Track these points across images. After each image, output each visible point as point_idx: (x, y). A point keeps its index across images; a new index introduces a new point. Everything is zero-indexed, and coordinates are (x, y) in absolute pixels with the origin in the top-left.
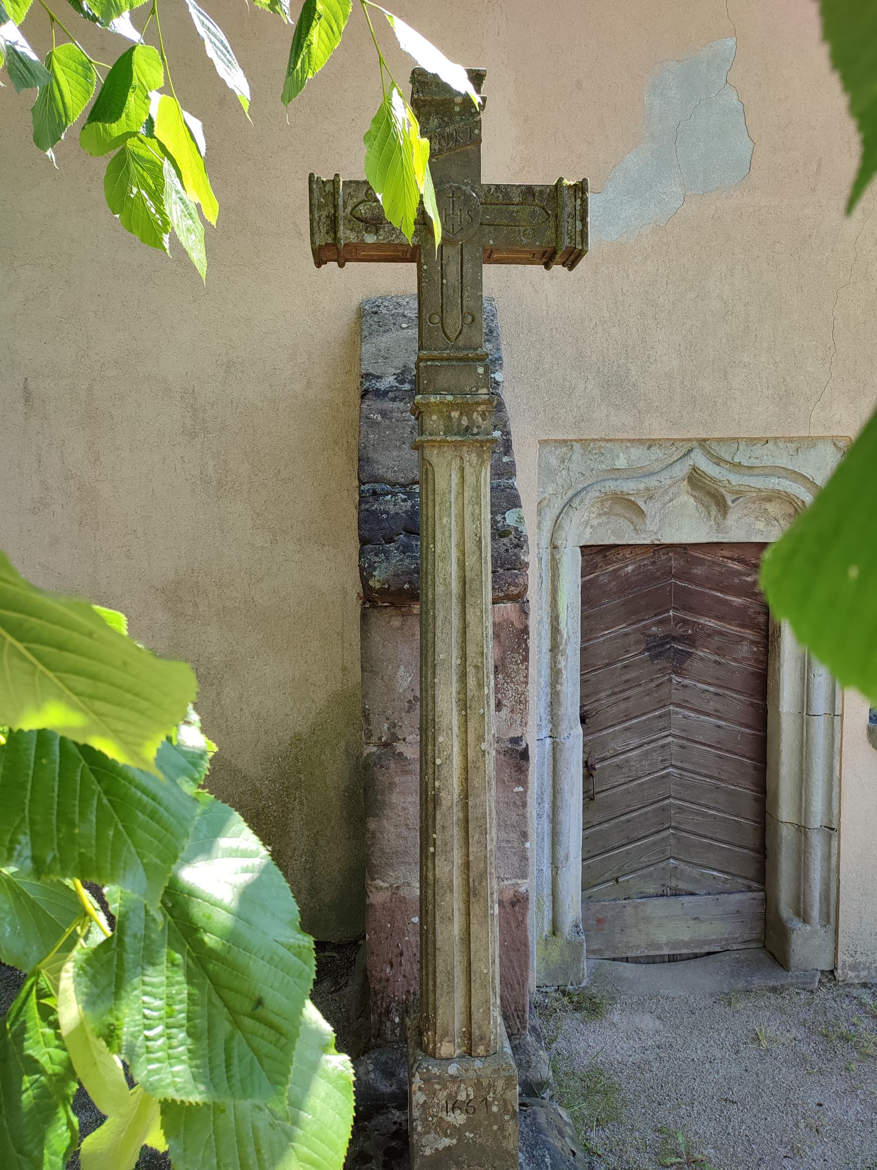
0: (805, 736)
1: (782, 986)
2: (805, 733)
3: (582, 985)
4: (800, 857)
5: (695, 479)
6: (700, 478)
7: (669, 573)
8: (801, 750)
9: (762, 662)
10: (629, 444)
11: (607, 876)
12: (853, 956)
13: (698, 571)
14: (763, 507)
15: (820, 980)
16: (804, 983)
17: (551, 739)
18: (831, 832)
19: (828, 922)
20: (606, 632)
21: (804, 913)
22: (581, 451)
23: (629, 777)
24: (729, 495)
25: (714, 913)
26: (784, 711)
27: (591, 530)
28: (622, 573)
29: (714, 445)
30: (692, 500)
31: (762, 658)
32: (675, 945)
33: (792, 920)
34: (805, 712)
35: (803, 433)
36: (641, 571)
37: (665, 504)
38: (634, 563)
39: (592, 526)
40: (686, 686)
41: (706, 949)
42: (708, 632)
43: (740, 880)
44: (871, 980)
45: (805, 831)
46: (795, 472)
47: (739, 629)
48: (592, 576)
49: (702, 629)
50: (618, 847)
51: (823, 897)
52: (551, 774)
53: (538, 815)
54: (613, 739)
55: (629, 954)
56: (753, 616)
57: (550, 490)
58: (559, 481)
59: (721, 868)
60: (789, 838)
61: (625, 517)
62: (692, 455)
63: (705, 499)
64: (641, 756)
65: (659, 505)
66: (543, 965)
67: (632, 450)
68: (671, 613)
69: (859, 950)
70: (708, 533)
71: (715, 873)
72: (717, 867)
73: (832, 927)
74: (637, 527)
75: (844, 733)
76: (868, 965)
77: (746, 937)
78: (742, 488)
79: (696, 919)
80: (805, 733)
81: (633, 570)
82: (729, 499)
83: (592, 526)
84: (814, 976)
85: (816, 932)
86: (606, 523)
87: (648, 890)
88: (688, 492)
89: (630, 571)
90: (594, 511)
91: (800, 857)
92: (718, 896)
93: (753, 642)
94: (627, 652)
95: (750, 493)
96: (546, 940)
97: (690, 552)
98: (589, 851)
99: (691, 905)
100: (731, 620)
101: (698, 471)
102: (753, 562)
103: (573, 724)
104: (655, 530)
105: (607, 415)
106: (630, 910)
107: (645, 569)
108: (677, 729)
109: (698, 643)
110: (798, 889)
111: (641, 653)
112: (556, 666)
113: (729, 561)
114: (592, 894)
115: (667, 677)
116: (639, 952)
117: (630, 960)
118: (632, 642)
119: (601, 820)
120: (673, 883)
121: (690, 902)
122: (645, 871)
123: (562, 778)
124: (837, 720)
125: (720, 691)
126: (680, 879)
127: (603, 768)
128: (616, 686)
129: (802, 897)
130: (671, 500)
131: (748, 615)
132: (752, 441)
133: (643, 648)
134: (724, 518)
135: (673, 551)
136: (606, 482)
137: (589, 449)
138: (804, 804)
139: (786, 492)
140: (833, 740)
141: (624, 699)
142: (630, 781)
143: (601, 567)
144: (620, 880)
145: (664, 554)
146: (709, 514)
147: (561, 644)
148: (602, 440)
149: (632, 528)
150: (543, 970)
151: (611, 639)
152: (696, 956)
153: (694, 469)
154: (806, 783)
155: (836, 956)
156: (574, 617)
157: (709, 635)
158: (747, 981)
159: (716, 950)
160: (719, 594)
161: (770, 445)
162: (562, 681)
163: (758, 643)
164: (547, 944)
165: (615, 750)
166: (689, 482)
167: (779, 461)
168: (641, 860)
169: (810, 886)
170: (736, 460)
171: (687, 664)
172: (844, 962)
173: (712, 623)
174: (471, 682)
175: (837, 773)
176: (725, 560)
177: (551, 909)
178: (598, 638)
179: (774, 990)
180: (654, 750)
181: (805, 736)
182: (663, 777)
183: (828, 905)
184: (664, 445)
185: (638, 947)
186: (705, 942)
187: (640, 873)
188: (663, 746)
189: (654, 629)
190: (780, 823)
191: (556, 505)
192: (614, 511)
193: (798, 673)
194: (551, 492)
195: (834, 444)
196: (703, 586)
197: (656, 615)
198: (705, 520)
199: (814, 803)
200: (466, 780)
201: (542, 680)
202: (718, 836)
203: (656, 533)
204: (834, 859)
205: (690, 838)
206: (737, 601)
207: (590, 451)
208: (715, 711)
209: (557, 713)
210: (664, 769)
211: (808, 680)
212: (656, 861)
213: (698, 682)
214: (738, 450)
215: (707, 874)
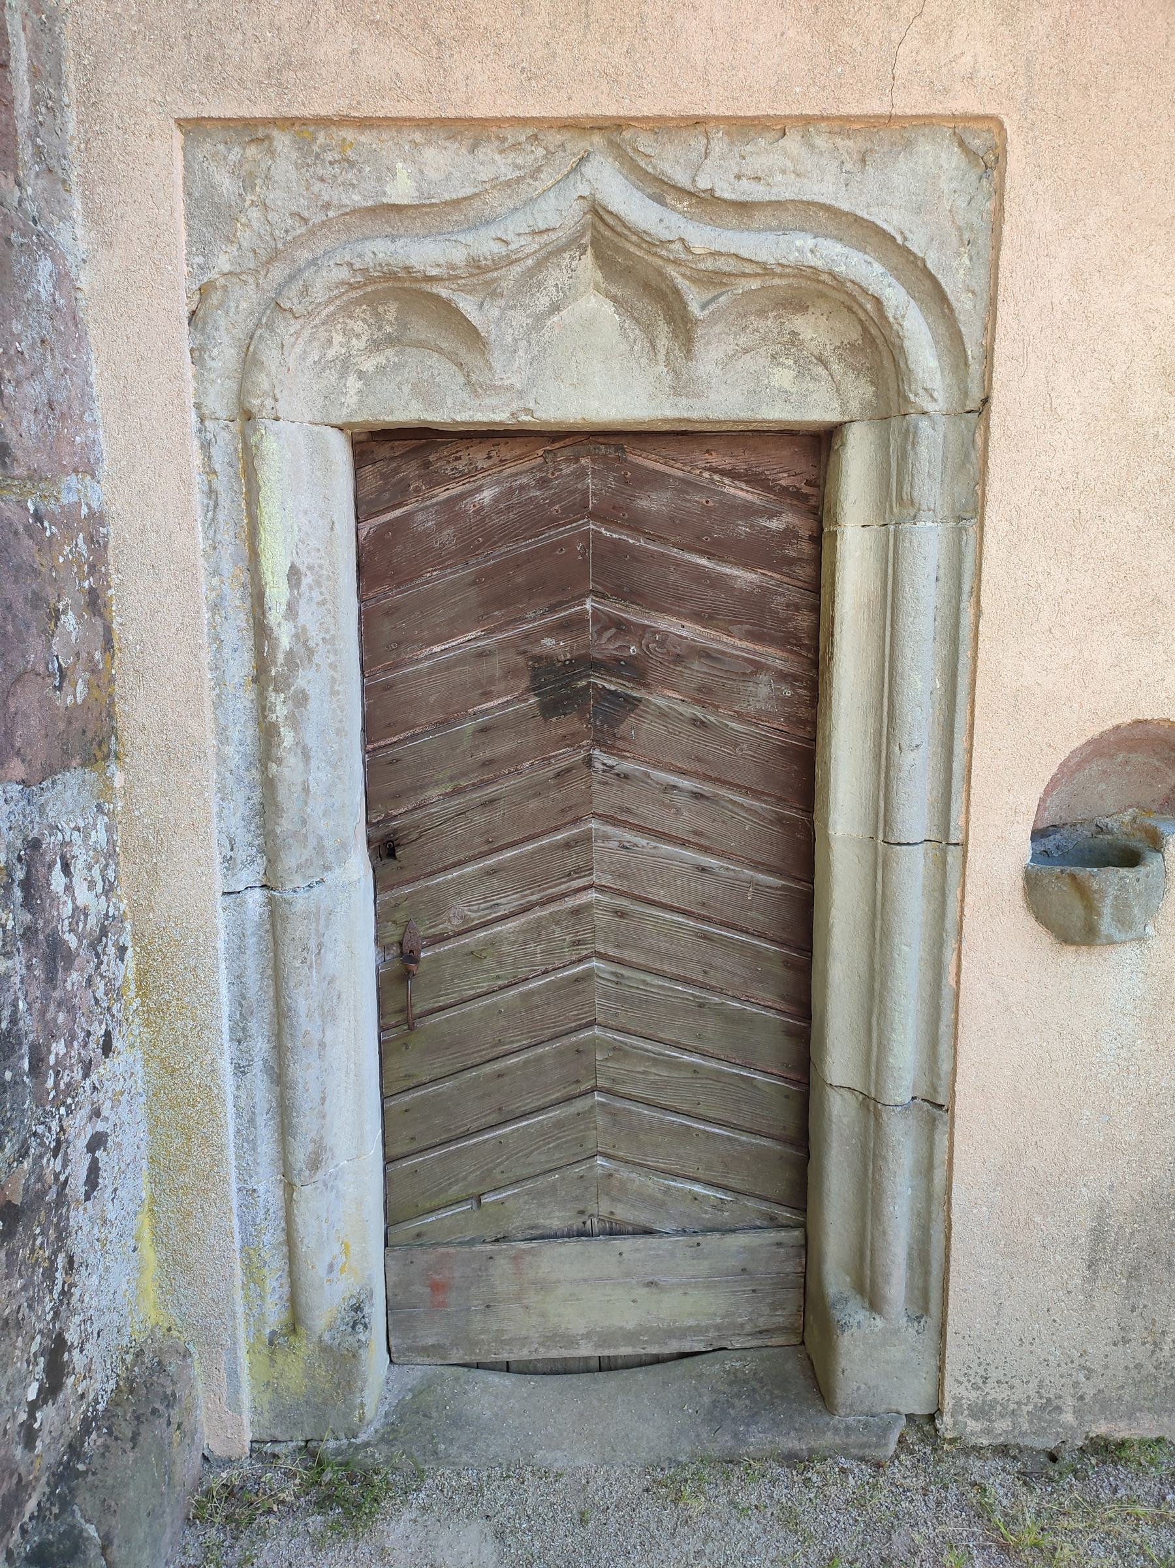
0: (880, 891)
1: (811, 1451)
2: (879, 887)
3: (358, 1441)
4: (865, 1166)
6: (616, 239)
7: (580, 509)
8: (873, 926)
9: (804, 722)
10: (418, 136)
11: (455, 1191)
12: (979, 1388)
13: (652, 503)
14: (788, 326)
15: (902, 1435)
16: (863, 1446)
17: (266, 892)
18: (937, 1112)
19: (926, 1310)
20: (436, 649)
21: (872, 1290)
22: (294, 155)
23: (498, 977)
24: (695, 289)
25: (691, 1273)
26: (839, 834)
27: (359, 384)
28: (468, 505)
29: (645, 143)
30: (609, 308)
31: (803, 713)
32: (605, 1338)
33: (846, 1300)
34: (881, 837)
35: (875, 106)
36: (515, 501)
37: (539, 320)
38: (498, 482)
39: (361, 375)
40: (626, 777)
41: (674, 1347)
42: (678, 651)
43: (751, 1203)
44: (1019, 1440)
45: (875, 1107)
46: (857, 219)
47: (751, 646)
48: (398, 513)
49: (662, 643)
50: (479, 1131)
51: (915, 1254)
52: (269, 972)
53: (237, 1067)
54: (458, 894)
55: (505, 1356)
56: (784, 614)
57: (223, 262)
58: (246, 237)
59: (712, 1176)
60: (845, 1121)
61: (440, 351)
62: (588, 170)
63: (639, 305)
64: (524, 932)
65: (520, 318)
66: (267, 1397)
67: (430, 153)
68: (588, 605)
69: (994, 1375)
70: (652, 397)
71: (698, 1189)
72: (701, 1174)
73: (932, 1322)
74: (473, 377)
75: (968, 887)
76: (1012, 1406)
77: (762, 1323)
78: (722, 264)
79: (651, 1284)
80: (879, 887)
81: (496, 500)
82: (694, 299)
83: (361, 375)
84: (886, 1429)
85: (896, 1331)
86: (399, 367)
87: (547, 1222)
88: (597, 288)
89: (486, 501)
90: (358, 330)
91: (865, 1166)
92: (700, 1239)
93: (782, 676)
94: (487, 695)
95: (743, 281)
96: (271, 1343)
97: (631, 458)
98: (413, 1139)
99: (638, 1255)
100: (732, 623)
101: (606, 216)
102: (783, 482)
103: (331, 857)
104: (519, 385)
105: (353, 52)
106: (502, 1266)
107: (524, 498)
108: (606, 872)
109: (652, 676)
110: (862, 1235)
111: (519, 699)
112: (265, 717)
113: (727, 481)
114: (424, 1229)
115: (583, 754)
116: (525, 1352)
117: (512, 1367)
118: (498, 673)
119: (437, 1072)
120: (604, 1207)
121: (637, 1250)
122: (540, 1183)
123: (292, 984)
124: (953, 854)
125: (706, 788)
126: (619, 1201)
127: (436, 959)
128: (464, 774)
129: (868, 1253)
130: (555, 308)
131: (771, 611)
133: (524, 686)
134: (688, 354)
135: (588, 453)
136: (367, 243)
137: (315, 148)
138: (875, 1049)
139: (831, 273)
140: (943, 903)
141: (484, 804)
142: (501, 988)
143: (417, 490)
144: (483, 1201)
145: (567, 460)
146: (653, 346)
147: (274, 663)
148: (344, 121)
149: (462, 380)
150: (266, 1407)
151: (448, 666)
152: (658, 1360)
153: (597, 211)
154: (881, 1001)
155: (940, 1384)
156: (323, 603)
157: (679, 659)
158: (735, 1435)
159: (696, 1350)
160: (703, 561)
161: (792, 143)
162: (281, 753)
163: (795, 678)
164: (273, 1353)
165: (466, 919)
166: (596, 257)
167: (816, 188)
168: (530, 1160)
169: (884, 1233)
170: (703, 183)
171: (628, 725)
172: (958, 1400)
175: (951, 979)
176: (716, 477)
177: (285, 1274)
178: (419, 661)
179: (791, 1459)
180: (555, 919)
181: (880, 891)
182: (578, 979)
183: (927, 1273)
184: (510, 141)
185: (524, 1341)
186: (672, 1333)
187: (529, 1185)
188: (576, 912)
189: (548, 642)
190: (828, 1089)
191: (244, 305)
192: (412, 335)
193: (869, 743)
194: (227, 268)
195: (962, 144)
196: (664, 541)
197: (553, 609)
198: (644, 361)
199: (896, 1048)
201: (229, 750)
202: (702, 1110)
203: (521, 394)
204: (939, 1175)
205: (639, 1114)
206: (745, 577)
207: (317, 156)
208: (695, 833)
209: (274, 831)
210: (580, 961)
211: (888, 758)
212: (561, 1163)
213: (655, 767)
214: (706, 155)
215: (678, 1190)
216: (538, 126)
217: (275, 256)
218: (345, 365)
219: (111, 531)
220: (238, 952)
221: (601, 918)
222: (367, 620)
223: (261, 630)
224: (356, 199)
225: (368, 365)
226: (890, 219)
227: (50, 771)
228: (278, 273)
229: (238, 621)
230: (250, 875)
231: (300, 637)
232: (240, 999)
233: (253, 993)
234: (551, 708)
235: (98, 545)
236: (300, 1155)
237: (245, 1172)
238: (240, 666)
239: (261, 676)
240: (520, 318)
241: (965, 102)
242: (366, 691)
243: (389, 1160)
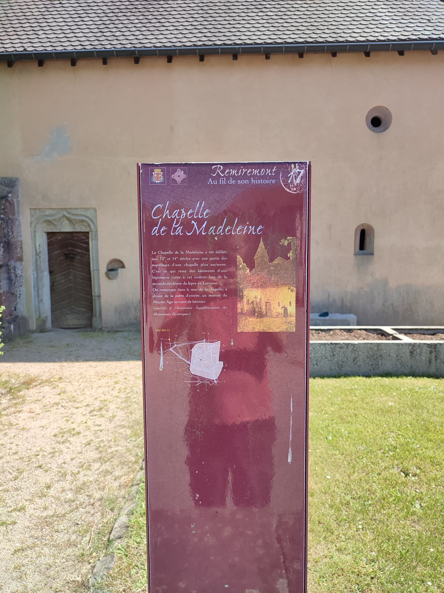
5: (64, 216)
37: (61, 223)
57: (33, 219)
132: (76, 209)
173: (79, 251)
216: (58, 209)
218: (44, 227)
219: (23, 242)
221: (72, 280)
223: (36, 250)
224: (44, 214)
226: (88, 215)
229: (34, 250)
231: (40, 251)
232: (34, 284)
234: (66, 258)
235: (22, 243)
236: (40, 300)
238: (34, 254)
239: (36, 255)
241: (93, 207)
243: (52, 305)
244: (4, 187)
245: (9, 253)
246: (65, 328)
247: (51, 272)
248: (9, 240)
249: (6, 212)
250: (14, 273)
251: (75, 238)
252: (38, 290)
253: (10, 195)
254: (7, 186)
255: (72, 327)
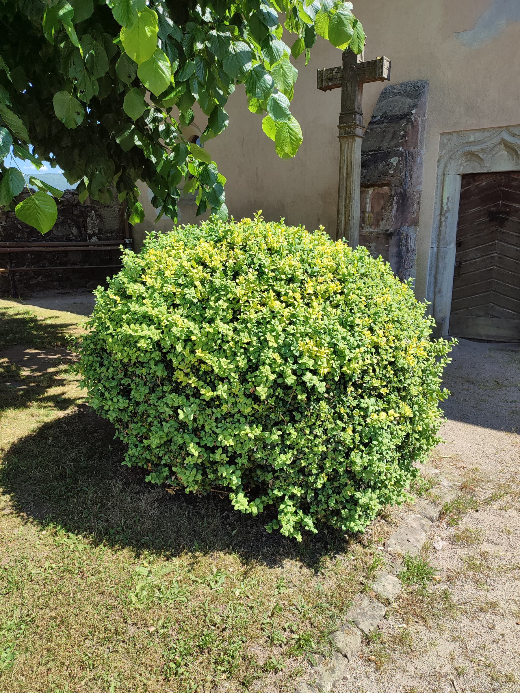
5: (504, 142)
13: (514, 183)
37: (493, 156)
41: (501, 340)
57: (444, 152)
58: (447, 148)
153: (503, 139)
174: (347, 201)
182: (490, 270)
200: (345, 227)
216: (494, 128)
217: (451, 151)
219: (422, 193)
220: (431, 257)
221: (496, 258)
222: (461, 205)
223: (442, 207)
225: (465, 165)
227: (410, 225)
228: (451, 153)
230: (435, 245)
231: (448, 208)
232: (431, 264)
233: (433, 263)
234: (491, 221)
235: (420, 195)
236: (437, 290)
237: (428, 292)
238: (438, 212)
240: (490, 156)
242: (459, 217)
244: (404, 99)
245: (403, 212)
246: (470, 339)
247: (459, 245)
248: (405, 190)
249: (406, 141)
250: (406, 246)
251: (514, 183)
252: (436, 273)
253: (413, 112)
254: (409, 96)
255: (484, 338)
